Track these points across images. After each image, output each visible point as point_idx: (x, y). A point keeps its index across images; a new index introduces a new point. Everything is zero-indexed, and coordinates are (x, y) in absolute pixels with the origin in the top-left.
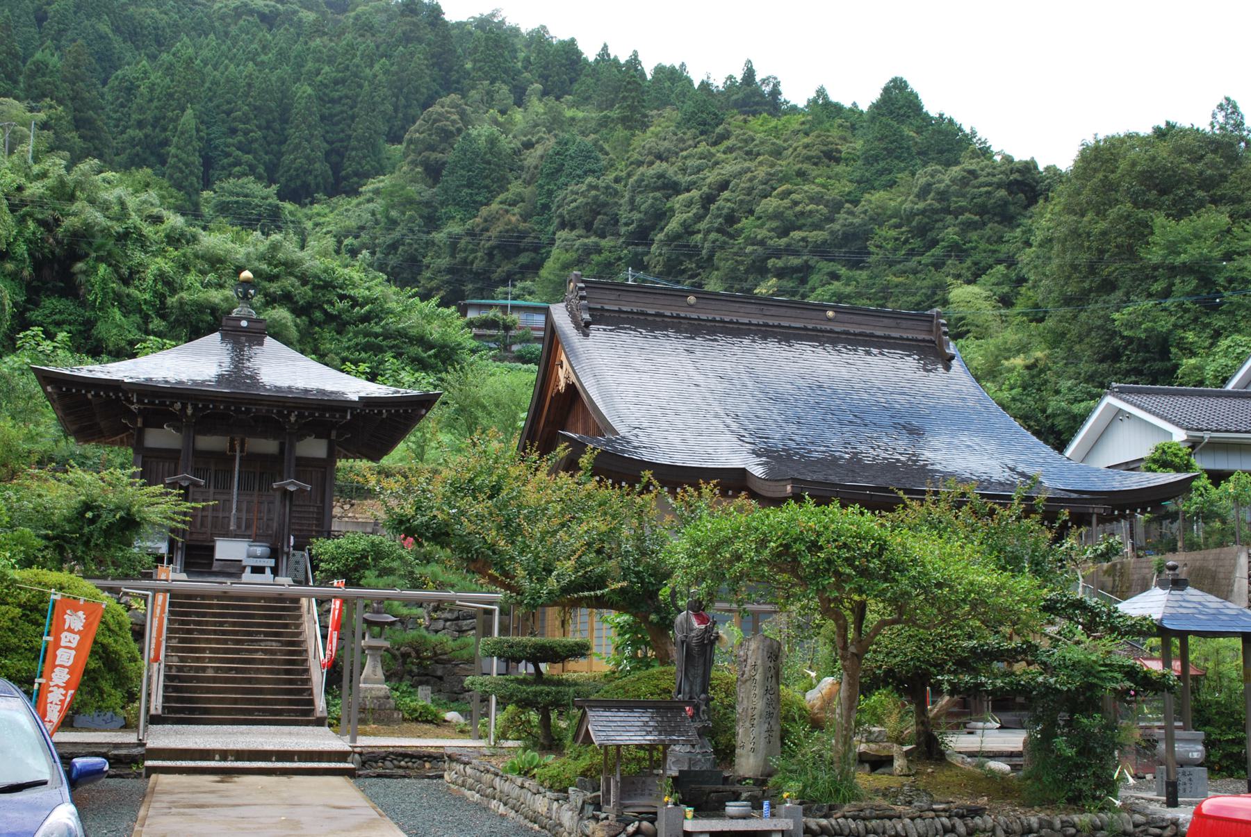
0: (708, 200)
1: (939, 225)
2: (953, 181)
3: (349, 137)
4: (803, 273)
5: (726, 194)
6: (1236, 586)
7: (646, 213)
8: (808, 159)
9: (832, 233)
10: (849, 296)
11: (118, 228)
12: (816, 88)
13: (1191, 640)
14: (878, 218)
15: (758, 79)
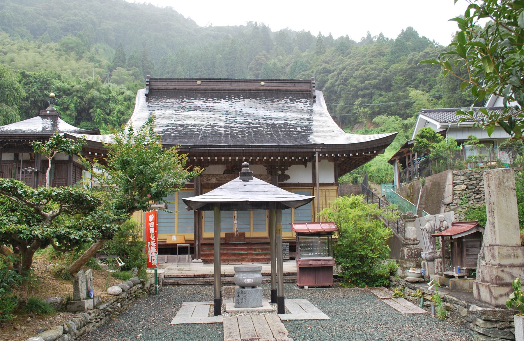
0: (340, 73)
1: (417, 73)
2: (421, 57)
3: (234, 70)
4: (371, 95)
5: (345, 71)
6: (446, 188)
7: (320, 82)
8: (373, 56)
9: (379, 80)
10: (385, 102)
11: (105, 97)
12: (380, 33)
13: (312, 222)
14: (395, 73)
15: (372, 37)
